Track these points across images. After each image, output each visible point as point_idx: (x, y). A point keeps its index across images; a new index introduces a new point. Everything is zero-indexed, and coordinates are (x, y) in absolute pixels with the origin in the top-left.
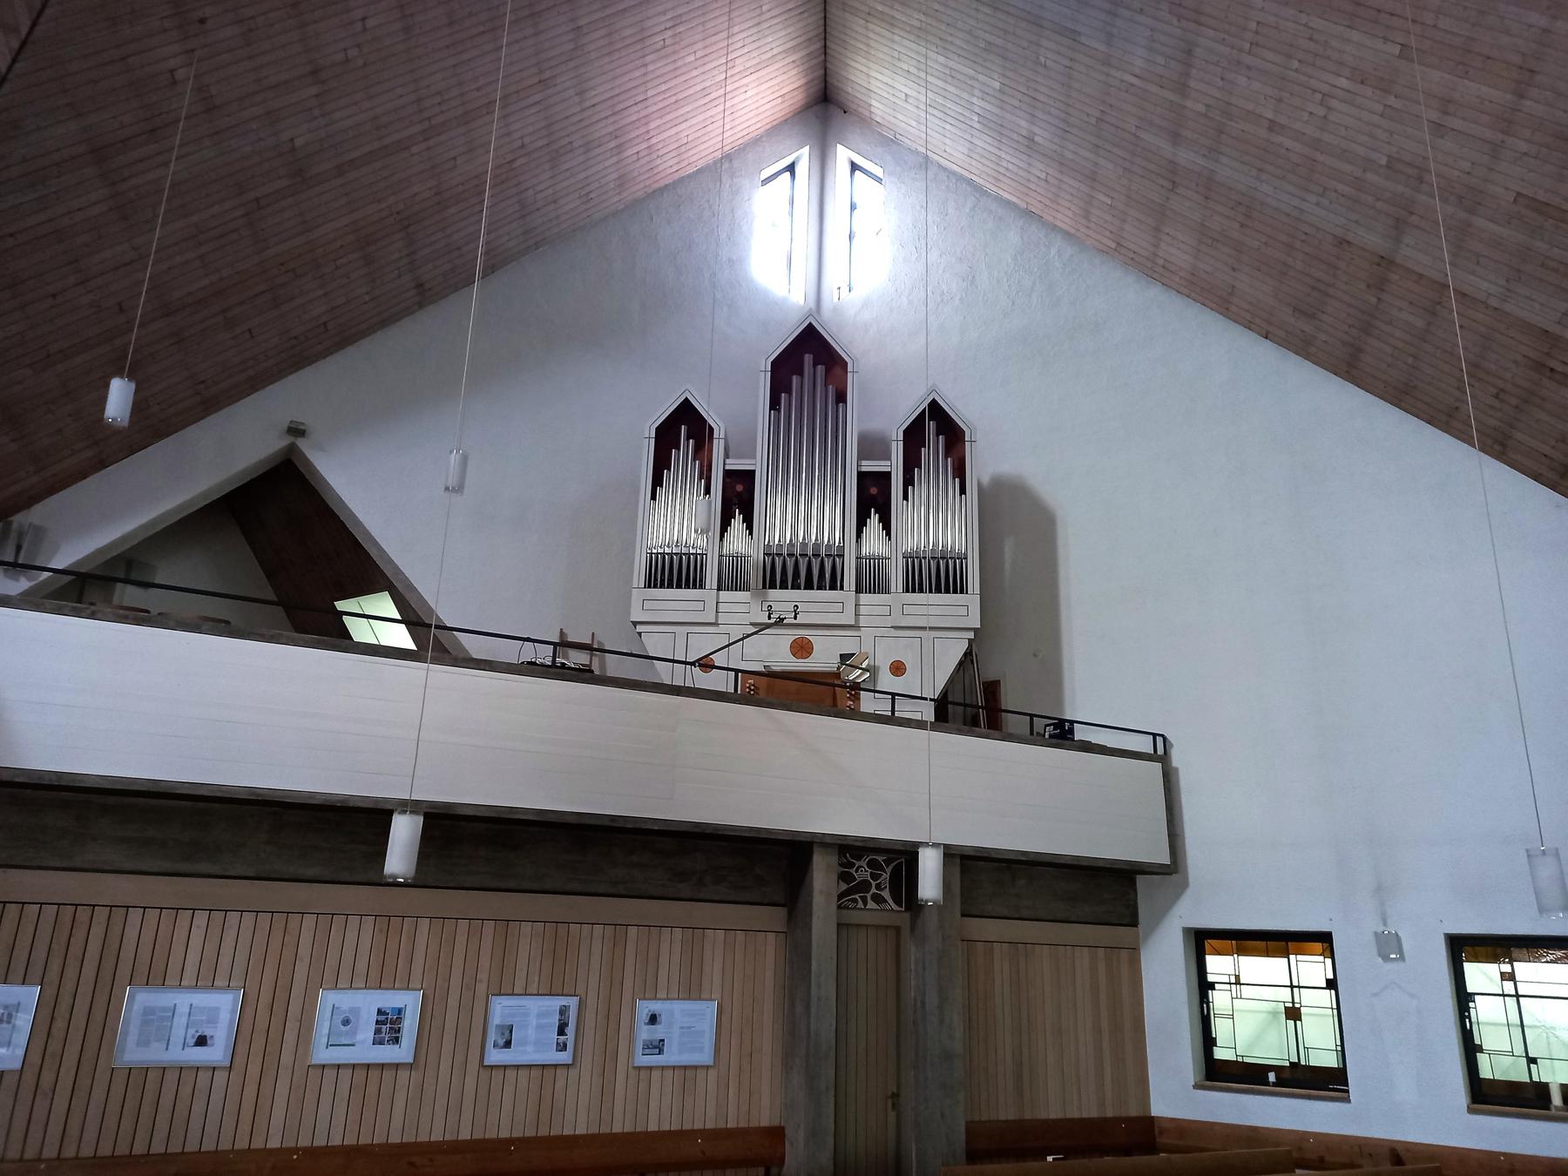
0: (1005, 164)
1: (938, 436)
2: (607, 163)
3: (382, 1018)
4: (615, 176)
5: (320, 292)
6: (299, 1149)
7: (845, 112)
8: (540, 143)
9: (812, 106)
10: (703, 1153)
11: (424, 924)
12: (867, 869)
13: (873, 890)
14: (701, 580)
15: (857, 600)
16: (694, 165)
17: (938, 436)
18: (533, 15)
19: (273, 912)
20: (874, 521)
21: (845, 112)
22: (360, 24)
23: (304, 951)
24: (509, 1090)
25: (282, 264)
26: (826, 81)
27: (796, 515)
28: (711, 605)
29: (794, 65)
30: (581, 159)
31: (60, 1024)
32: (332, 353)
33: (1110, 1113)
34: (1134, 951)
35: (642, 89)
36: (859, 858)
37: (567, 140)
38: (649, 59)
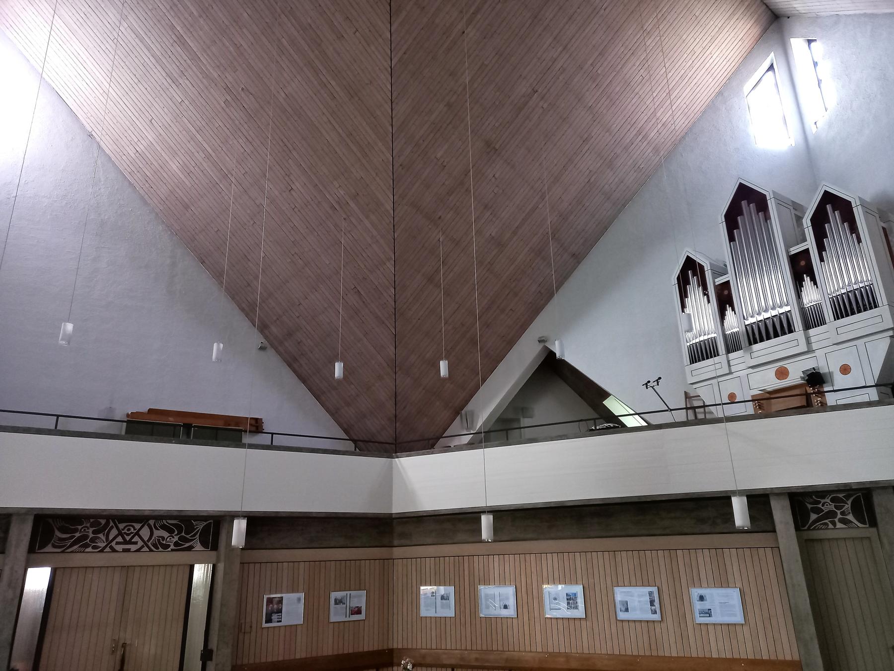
1: (834, 213)
6: (548, 652)
7: (788, 18)
12: (831, 503)
13: (839, 516)
14: (717, 351)
15: (728, 358)
17: (834, 213)
23: (534, 570)
25: (510, 280)
26: (770, 9)
28: (802, 341)
31: (462, 600)
32: (549, 301)
35: (642, 103)
36: (824, 498)
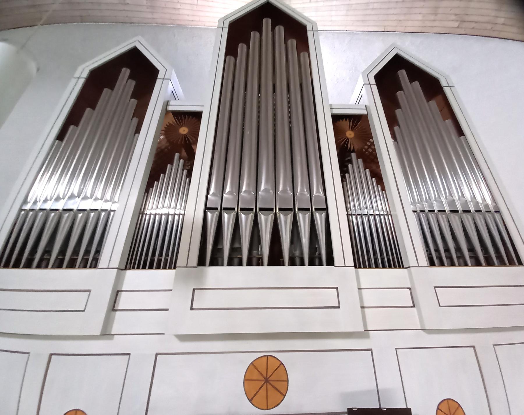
0: (371, 7)
14: (98, 252)
15: (119, 280)
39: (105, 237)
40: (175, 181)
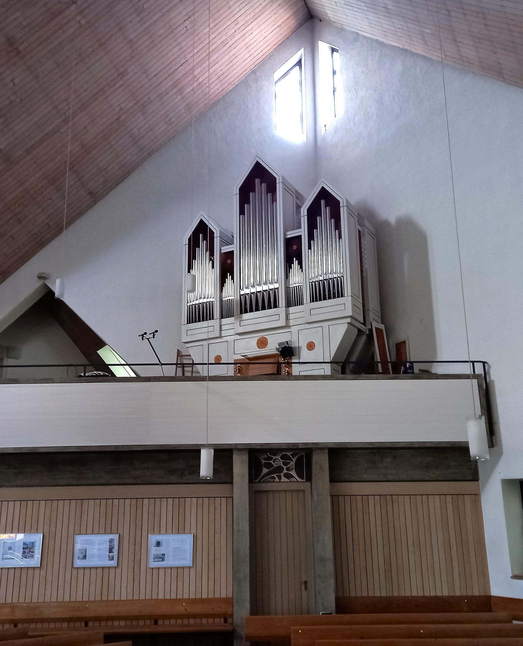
1: (326, 208)
2: (176, 101)
3: (25, 546)
4: (183, 105)
5: (39, 210)
7: (321, 21)
8: (131, 105)
9: (303, 24)
10: (186, 610)
11: (224, 500)
12: (280, 460)
13: (285, 471)
15: (220, 322)
16: (233, 83)
17: (326, 208)
18: (101, 45)
19: (143, 498)
20: (295, 264)
21: (321, 21)
22: (11, 83)
24: (87, 578)
25: (15, 203)
26: (307, 7)
27: (327, 260)
29: (280, 7)
30: (159, 104)
33: (458, 593)
34: (476, 497)
36: (275, 455)
37: (146, 98)
38: (179, 40)
39: (220, 312)
40: (327, 224)
